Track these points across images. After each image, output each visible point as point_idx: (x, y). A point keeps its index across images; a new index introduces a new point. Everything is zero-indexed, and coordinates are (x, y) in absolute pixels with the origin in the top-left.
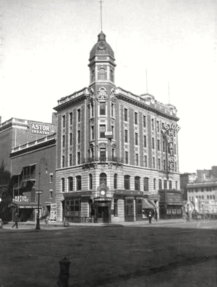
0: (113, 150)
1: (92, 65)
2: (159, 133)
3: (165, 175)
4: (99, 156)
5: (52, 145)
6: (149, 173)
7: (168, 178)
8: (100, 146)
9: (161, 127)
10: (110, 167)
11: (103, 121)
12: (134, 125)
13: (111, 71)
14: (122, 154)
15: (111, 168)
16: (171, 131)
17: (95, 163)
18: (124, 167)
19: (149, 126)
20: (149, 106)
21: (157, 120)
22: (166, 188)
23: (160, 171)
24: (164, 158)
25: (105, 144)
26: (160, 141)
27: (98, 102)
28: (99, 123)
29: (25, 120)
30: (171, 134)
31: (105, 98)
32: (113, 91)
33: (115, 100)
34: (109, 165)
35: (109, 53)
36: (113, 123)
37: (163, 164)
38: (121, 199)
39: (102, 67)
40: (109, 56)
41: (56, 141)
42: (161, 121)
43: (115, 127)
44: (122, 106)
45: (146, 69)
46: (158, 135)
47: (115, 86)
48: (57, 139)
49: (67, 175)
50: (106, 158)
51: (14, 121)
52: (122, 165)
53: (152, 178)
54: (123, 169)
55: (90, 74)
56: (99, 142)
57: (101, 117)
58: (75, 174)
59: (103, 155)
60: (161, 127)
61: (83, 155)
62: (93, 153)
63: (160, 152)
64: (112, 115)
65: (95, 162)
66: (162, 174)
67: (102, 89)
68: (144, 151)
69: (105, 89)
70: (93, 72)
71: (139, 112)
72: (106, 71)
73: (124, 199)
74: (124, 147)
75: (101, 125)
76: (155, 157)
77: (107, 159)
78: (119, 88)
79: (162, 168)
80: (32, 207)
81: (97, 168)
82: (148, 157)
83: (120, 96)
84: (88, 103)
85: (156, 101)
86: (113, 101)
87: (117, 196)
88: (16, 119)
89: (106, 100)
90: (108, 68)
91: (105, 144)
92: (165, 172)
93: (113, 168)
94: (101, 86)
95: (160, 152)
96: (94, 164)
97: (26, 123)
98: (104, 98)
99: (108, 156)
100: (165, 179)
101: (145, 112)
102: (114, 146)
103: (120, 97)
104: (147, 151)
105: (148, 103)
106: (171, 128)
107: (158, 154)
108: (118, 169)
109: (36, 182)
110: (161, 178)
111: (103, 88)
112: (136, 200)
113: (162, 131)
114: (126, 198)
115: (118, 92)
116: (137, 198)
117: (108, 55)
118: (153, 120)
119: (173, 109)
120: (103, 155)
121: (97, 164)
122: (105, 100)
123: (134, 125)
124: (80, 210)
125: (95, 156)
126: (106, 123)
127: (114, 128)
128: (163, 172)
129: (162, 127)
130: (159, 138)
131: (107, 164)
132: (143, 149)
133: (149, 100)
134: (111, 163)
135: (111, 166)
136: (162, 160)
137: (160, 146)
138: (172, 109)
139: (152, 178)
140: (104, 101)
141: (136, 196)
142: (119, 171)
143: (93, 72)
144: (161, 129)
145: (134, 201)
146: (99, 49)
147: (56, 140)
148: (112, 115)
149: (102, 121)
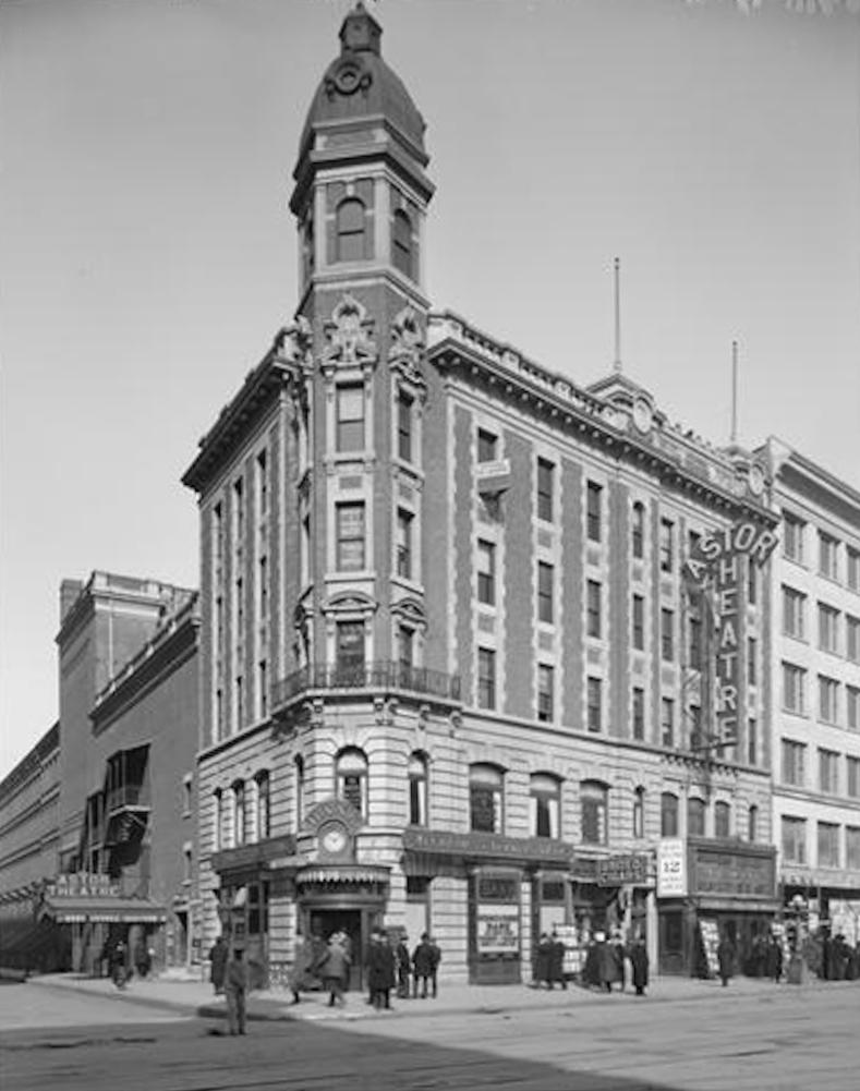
0: (408, 632)
1: (301, 203)
2: (674, 579)
3: (693, 773)
4: (331, 657)
5: (186, 652)
6: (613, 762)
7: (708, 789)
8: (336, 612)
9: (682, 551)
10: (385, 715)
11: (353, 483)
12: (535, 519)
13: (399, 213)
14: (464, 661)
15: (391, 724)
16: (729, 565)
17: (310, 699)
18: (467, 722)
19: (617, 534)
20: (621, 433)
21: (665, 511)
22: (702, 831)
23: (669, 756)
24: (694, 699)
25: (360, 601)
26: (677, 616)
27: (328, 381)
28: (335, 493)
29: (147, 582)
30: (729, 575)
31: (364, 360)
32: (410, 326)
33: (418, 374)
34: (379, 708)
35: (384, 109)
36: (405, 492)
37: (690, 724)
38: (447, 875)
39: (350, 191)
40: (386, 126)
41: (198, 626)
42: (682, 520)
43: (423, 516)
44: (464, 418)
45: (617, 260)
46: (668, 589)
47: (426, 305)
48: (199, 620)
49: (223, 775)
50: (363, 674)
51: (100, 585)
52: (458, 709)
53: (623, 783)
54: (458, 734)
55: (300, 249)
56: (332, 590)
57: (339, 463)
58: (252, 766)
59: (351, 660)
60: (682, 551)
61: (275, 667)
62: (307, 656)
63: (674, 667)
64: (405, 453)
65: (309, 693)
66: (681, 771)
67: (348, 311)
68: (585, 656)
69: (362, 311)
70: (308, 228)
71: (567, 464)
72: (369, 212)
73: (470, 878)
74: (474, 624)
75: (340, 505)
76: (646, 685)
77: (369, 678)
78: (448, 316)
79: (681, 741)
80: (121, 915)
81: (321, 725)
82: (606, 686)
83: (449, 355)
84: (292, 416)
85: (659, 419)
86: (406, 379)
87: (425, 864)
88: (109, 576)
89: (368, 370)
90: (382, 192)
91: (360, 601)
92: (694, 760)
93: (398, 721)
94: (335, 295)
95: (674, 667)
96: (307, 705)
97: (152, 593)
98: (356, 362)
99: (377, 662)
100: (696, 791)
101: (595, 465)
102: (409, 612)
103: (449, 362)
104: (604, 656)
105: (614, 420)
106: (728, 547)
107: (663, 678)
108: (430, 727)
109: (151, 818)
110: (674, 788)
111: (350, 301)
112: (533, 881)
113: (685, 571)
114: (477, 871)
115: (437, 334)
116: (539, 874)
117: (381, 116)
118: (638, 506)
119: (751, 471)
120: (351, 660)
121: (318, 702)
122: (362, 367)
123: (535, 520)
124: (266, 929)
125: (316, 665)
126: (365, 493)
127: (416, 524)
128: (686, 759)
129: (687, 549)
130: (673, 602)
131: (369, 699)
132: (580, 646)
133: (625, 407)
134: (387, 697)
135: (393, 709)
136: (683, 704)
137: (676, 639)
138: (743, 469)
139: (623, 783)
140: (357, 375)
141: (531, 868)
142: (434, 737)
143: (308, 228)
144: (682, 556)
145: (526, 887)
146: (337, 89)
147: (196, 623)
148: (405, 453)
149: (349, 483)
